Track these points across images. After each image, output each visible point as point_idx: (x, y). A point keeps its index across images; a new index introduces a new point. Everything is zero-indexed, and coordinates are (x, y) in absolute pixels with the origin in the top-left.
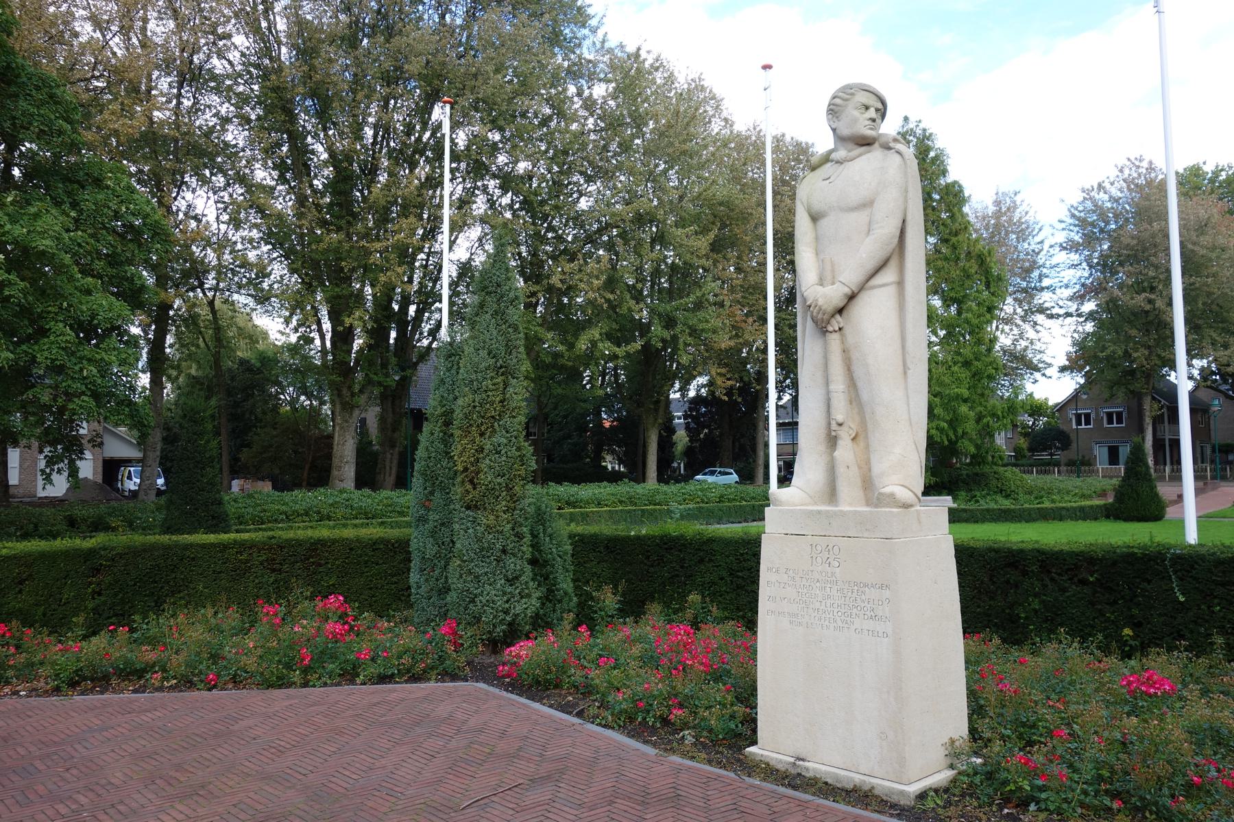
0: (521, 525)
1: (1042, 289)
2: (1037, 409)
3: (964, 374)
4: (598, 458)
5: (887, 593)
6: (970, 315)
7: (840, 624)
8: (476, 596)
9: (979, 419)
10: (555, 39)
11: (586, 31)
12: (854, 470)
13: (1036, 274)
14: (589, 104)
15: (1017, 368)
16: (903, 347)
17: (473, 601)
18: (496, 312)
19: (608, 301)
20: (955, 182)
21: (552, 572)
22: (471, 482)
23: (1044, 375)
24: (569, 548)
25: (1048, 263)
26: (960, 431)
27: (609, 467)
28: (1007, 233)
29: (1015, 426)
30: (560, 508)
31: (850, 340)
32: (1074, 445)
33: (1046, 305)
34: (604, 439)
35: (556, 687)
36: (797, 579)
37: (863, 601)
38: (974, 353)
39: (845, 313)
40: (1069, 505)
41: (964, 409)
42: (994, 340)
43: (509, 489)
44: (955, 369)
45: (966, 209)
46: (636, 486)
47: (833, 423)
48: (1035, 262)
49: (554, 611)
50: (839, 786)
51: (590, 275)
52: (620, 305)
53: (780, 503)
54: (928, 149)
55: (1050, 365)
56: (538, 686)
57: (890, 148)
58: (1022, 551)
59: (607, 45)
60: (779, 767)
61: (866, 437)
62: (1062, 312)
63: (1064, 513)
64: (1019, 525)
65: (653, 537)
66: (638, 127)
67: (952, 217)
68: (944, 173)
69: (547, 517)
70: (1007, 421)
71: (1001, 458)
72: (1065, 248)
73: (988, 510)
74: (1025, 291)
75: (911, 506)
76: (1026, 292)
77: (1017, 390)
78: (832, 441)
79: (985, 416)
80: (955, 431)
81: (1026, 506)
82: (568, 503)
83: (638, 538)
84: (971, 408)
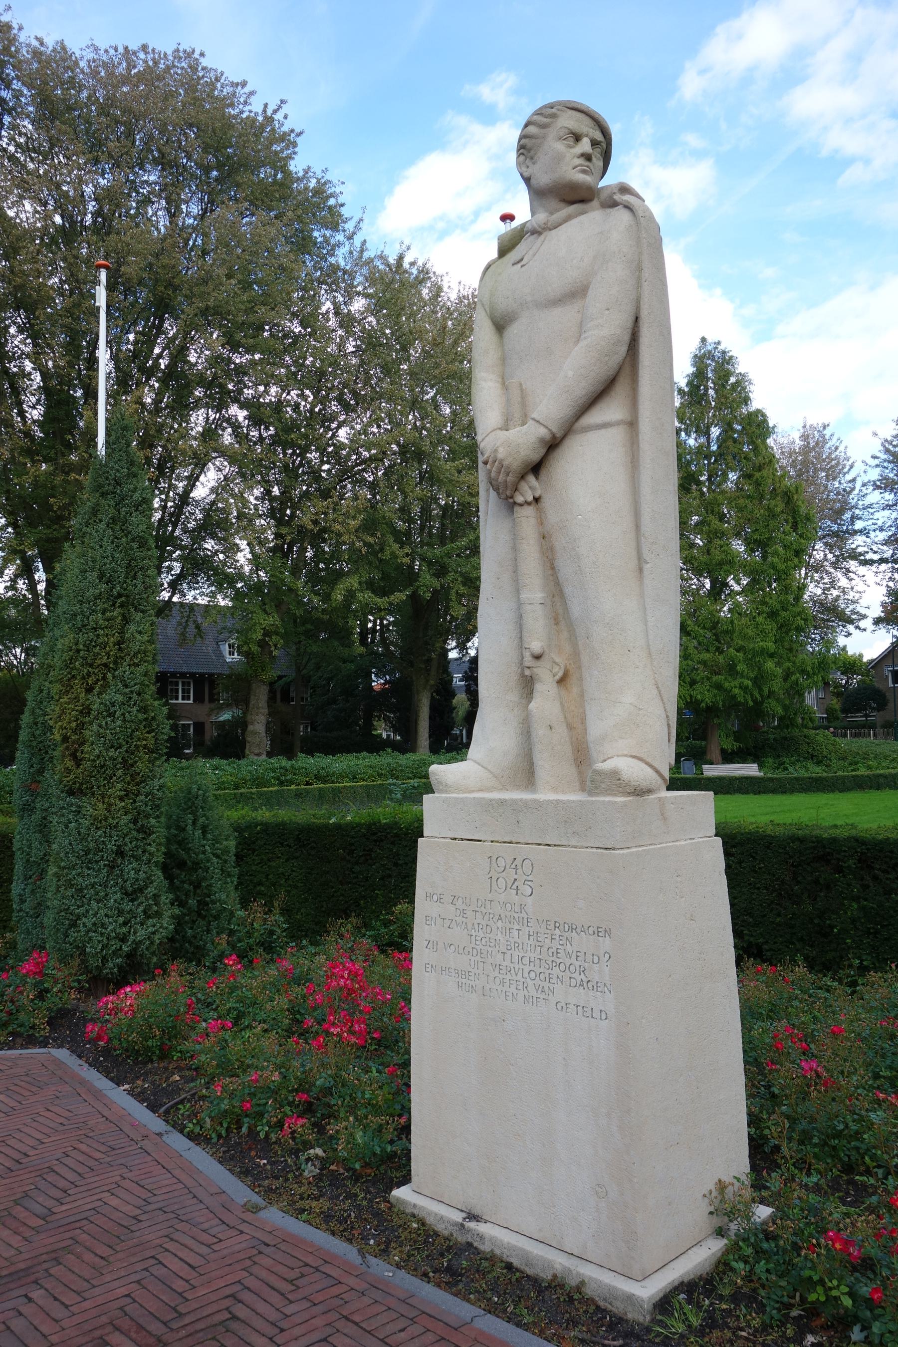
0: (147, 816)
1: (855, 532)
2: (851, 666)
3: (770, 626)
4: (369, 726)
5: (606, 943)
6: (775, 560)
7: (533, 992)
8: (79, 918)
9: (787, 676)
10: (303, 244)
11: (340, 237)
12: (561, 731)
13: (847, 515)
14: (347, 322)
15: (828, 620)
16: (637, 527)
17: (74, 925)
18: (114, 520)
19: (366, 544)
20: (759, 411)
21: (205, 879)
22: (74, 756)
23: (858, 627)
24: (232, 844)
25: (860, 503)
26: (766, 690)
27: (384, 736)
28: (816, 471)
29: (827, 684)
30: (308, 784)
31: (552, 517)
32: (891, 705)
33: (860, 550)
34: (376, 703)
35: (162, 1058)
36: (469, 913)
37: (569, 955)
38: (781, 602)
39: (543, 473)
40: (887, 771)
41: (770, 665)
42: (803, 588)
43: (126, 765)
44: (760, 619)
45: (770, 441)
46: (401, 756)
47: (527, 654)
48: (846, 502)
49: (208, 931)
50: (529, 1271)
51: (346, 515)
52: (382, 550)
53: (446, 789)
54: (728, 374)
55: (864, 617)
56: (122, 1061)
57: (614, 204)
58: (834, 840)
59: (366, 255)
60: (440, 1228)
61: (581, 679)
62: (876, 557)
63: (882, 780)
64: (831, 795)
65: (359, 825)
66: (405, 349)
67: (755, 450)
68: (746, 400)
69: (198, 802)
70: (818, 678)
71: (811, 720)
72: (879, 487)
73: (797, 779)
74: (836, 534)
75: (650, 791)
76: (838, 536)
77: (830, 644)
78: (527, 685)
79: (793, 673)
80: (760, 690)
81: (840, 773)
82: (318, 778)
83: (338, 827)
84: (778, 664)
